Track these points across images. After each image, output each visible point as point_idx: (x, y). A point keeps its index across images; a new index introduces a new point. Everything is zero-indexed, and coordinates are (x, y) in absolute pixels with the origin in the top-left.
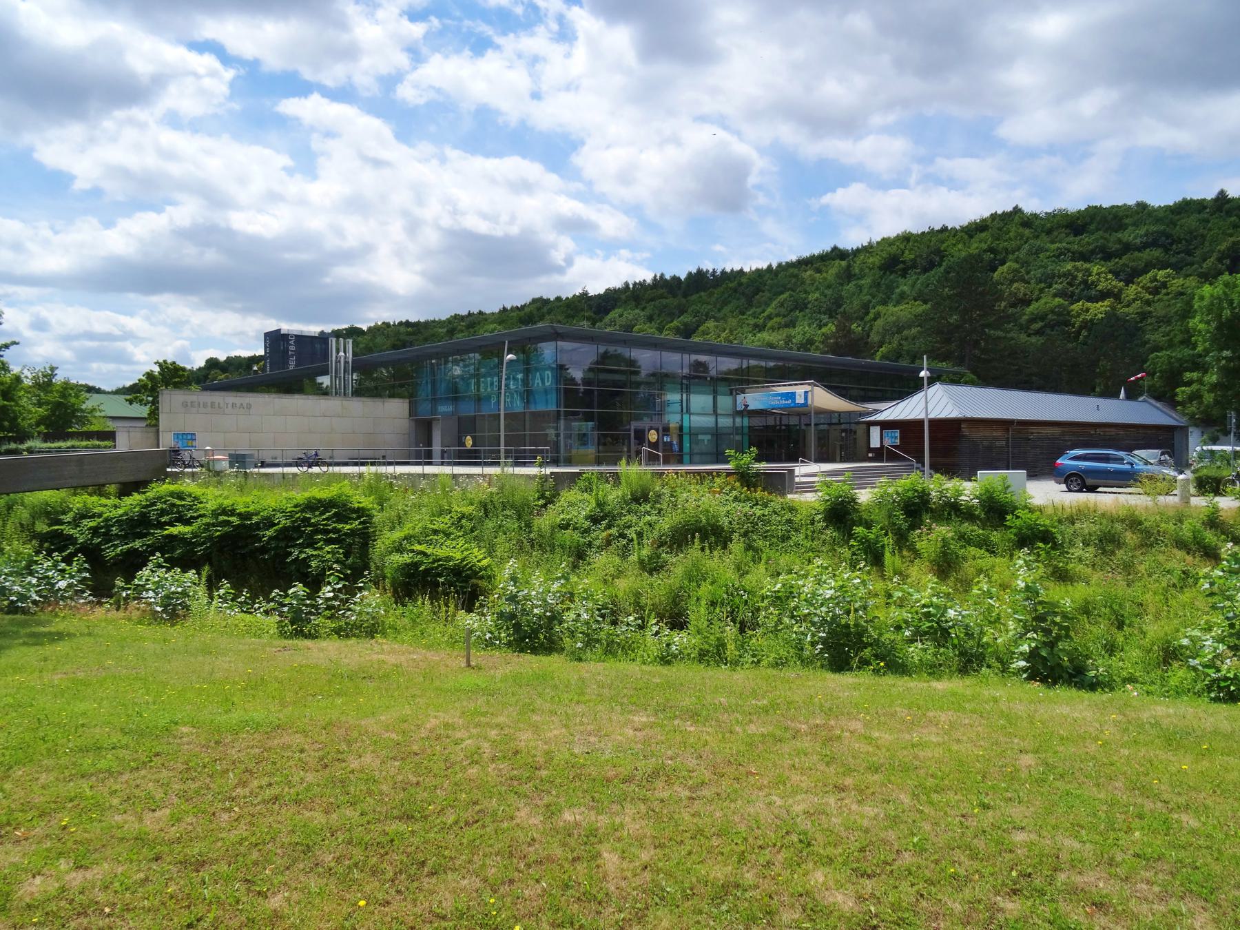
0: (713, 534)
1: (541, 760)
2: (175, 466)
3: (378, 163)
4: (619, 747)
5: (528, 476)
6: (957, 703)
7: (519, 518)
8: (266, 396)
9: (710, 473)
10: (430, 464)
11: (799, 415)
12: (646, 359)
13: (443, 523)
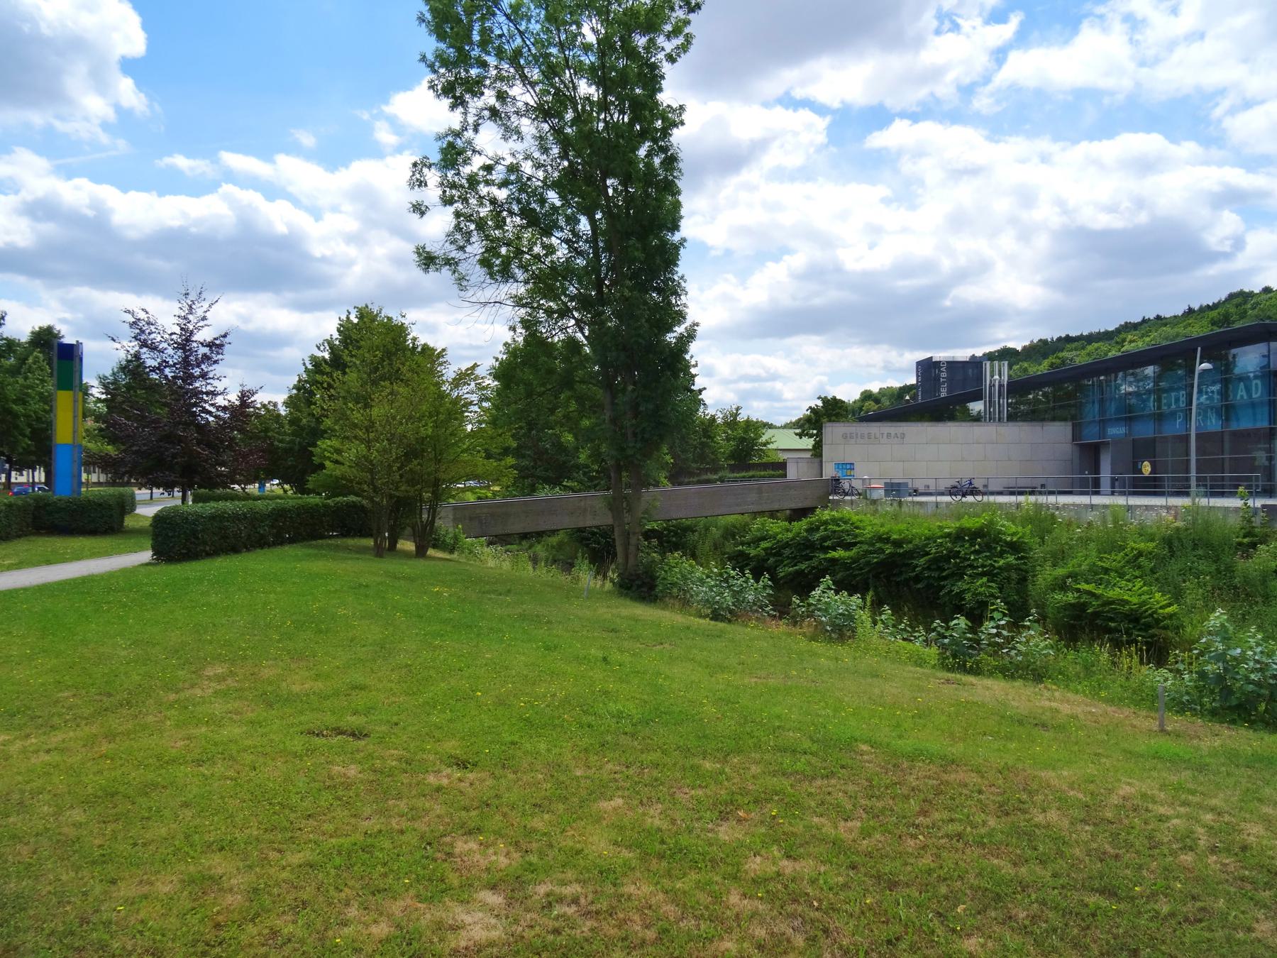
2: (836, 493)
3: (973, 171)
5: (1226, 509)
8: (919, 424)
10: (1097, 493)
13: (1114, 560)
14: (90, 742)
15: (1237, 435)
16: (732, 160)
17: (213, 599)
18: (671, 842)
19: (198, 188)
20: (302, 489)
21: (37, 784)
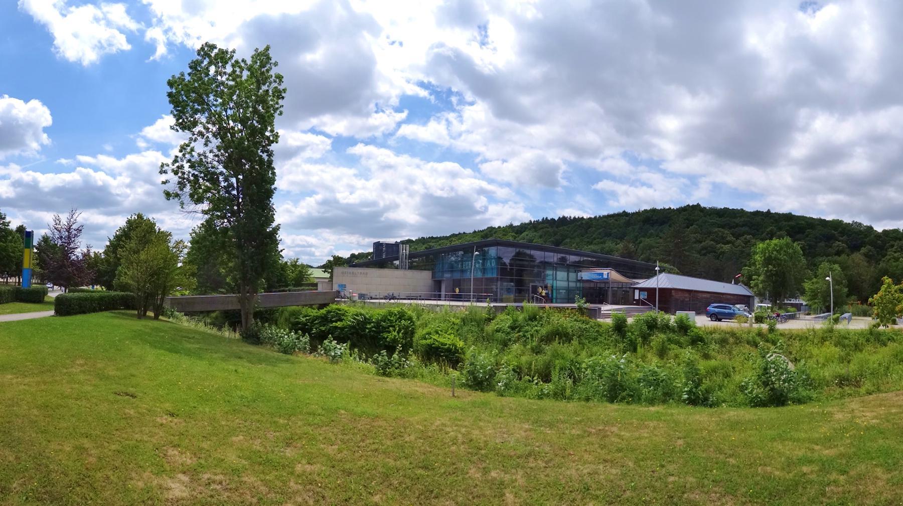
0: (563, 336)
1: (482, 445)
4: (517, 441)
6: (658, 417)
7: (478, 326)
9: (564, 308)
11: (605, 283)
12: (538, 255)
14: (38, 383)
15: (487, 279)
16: (291, 153)
17: (77, 332)
18: (264, 457)
19: (70, 170)
20: (109, 287)
21: (22, 397)
